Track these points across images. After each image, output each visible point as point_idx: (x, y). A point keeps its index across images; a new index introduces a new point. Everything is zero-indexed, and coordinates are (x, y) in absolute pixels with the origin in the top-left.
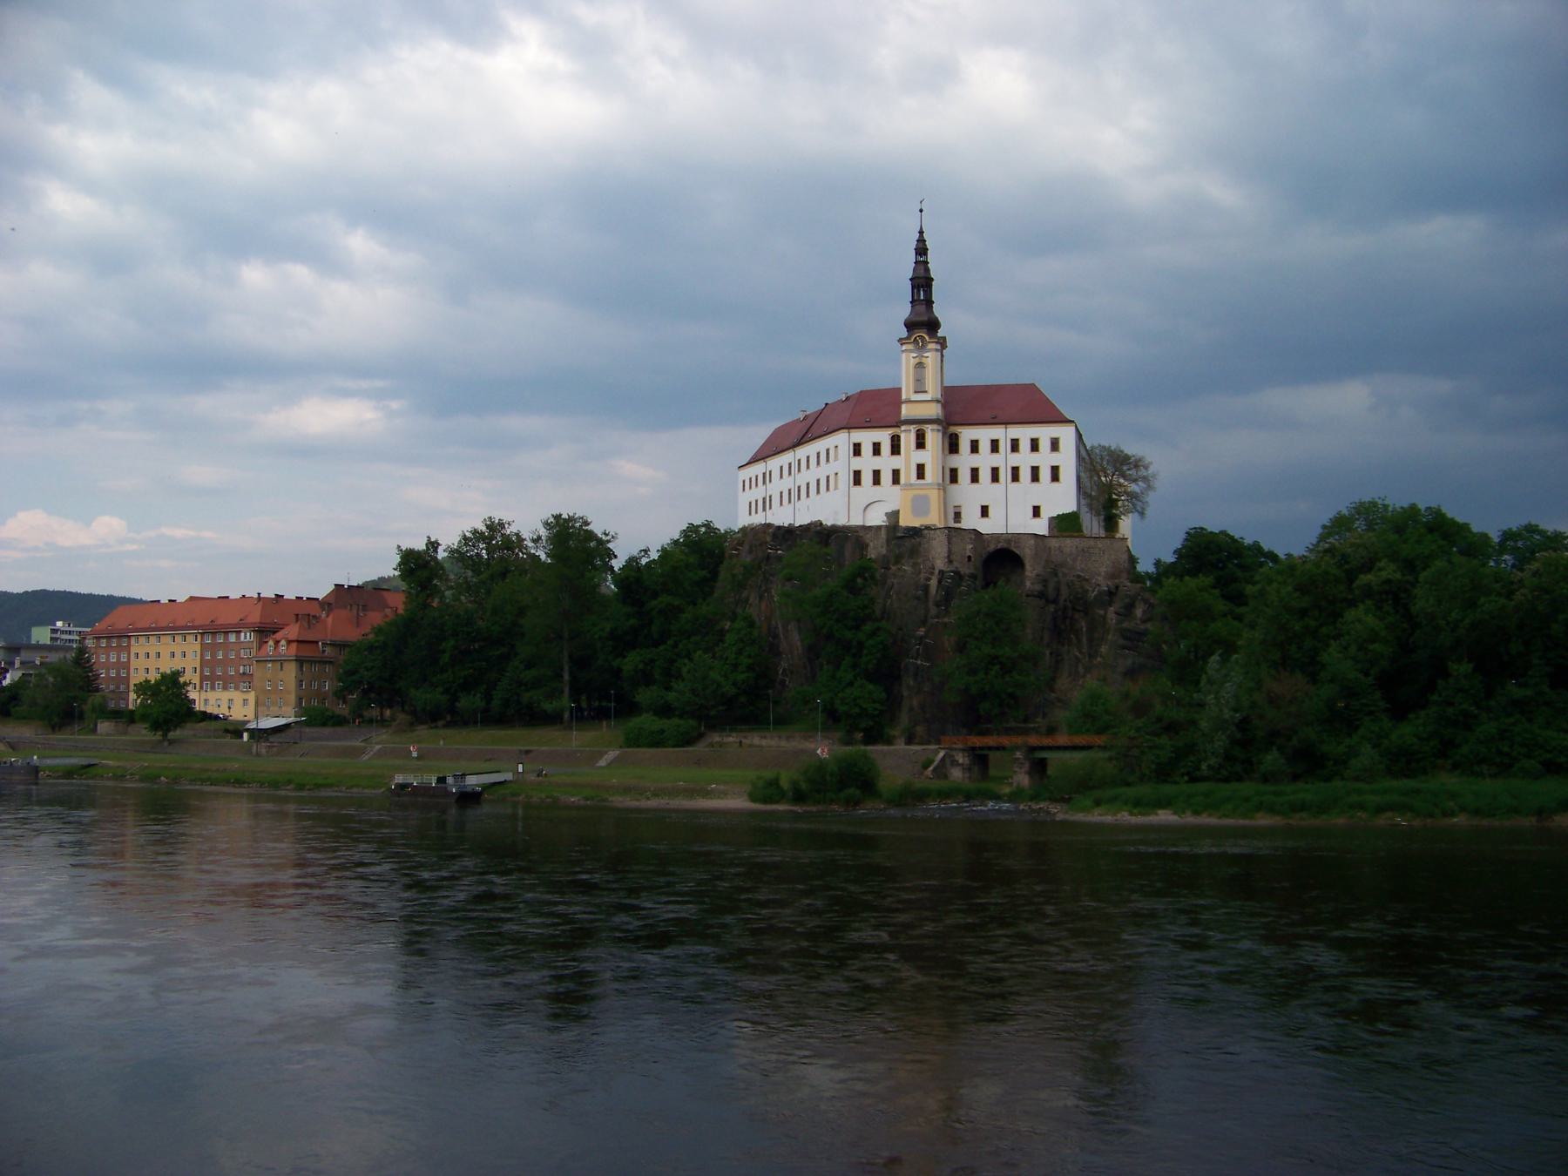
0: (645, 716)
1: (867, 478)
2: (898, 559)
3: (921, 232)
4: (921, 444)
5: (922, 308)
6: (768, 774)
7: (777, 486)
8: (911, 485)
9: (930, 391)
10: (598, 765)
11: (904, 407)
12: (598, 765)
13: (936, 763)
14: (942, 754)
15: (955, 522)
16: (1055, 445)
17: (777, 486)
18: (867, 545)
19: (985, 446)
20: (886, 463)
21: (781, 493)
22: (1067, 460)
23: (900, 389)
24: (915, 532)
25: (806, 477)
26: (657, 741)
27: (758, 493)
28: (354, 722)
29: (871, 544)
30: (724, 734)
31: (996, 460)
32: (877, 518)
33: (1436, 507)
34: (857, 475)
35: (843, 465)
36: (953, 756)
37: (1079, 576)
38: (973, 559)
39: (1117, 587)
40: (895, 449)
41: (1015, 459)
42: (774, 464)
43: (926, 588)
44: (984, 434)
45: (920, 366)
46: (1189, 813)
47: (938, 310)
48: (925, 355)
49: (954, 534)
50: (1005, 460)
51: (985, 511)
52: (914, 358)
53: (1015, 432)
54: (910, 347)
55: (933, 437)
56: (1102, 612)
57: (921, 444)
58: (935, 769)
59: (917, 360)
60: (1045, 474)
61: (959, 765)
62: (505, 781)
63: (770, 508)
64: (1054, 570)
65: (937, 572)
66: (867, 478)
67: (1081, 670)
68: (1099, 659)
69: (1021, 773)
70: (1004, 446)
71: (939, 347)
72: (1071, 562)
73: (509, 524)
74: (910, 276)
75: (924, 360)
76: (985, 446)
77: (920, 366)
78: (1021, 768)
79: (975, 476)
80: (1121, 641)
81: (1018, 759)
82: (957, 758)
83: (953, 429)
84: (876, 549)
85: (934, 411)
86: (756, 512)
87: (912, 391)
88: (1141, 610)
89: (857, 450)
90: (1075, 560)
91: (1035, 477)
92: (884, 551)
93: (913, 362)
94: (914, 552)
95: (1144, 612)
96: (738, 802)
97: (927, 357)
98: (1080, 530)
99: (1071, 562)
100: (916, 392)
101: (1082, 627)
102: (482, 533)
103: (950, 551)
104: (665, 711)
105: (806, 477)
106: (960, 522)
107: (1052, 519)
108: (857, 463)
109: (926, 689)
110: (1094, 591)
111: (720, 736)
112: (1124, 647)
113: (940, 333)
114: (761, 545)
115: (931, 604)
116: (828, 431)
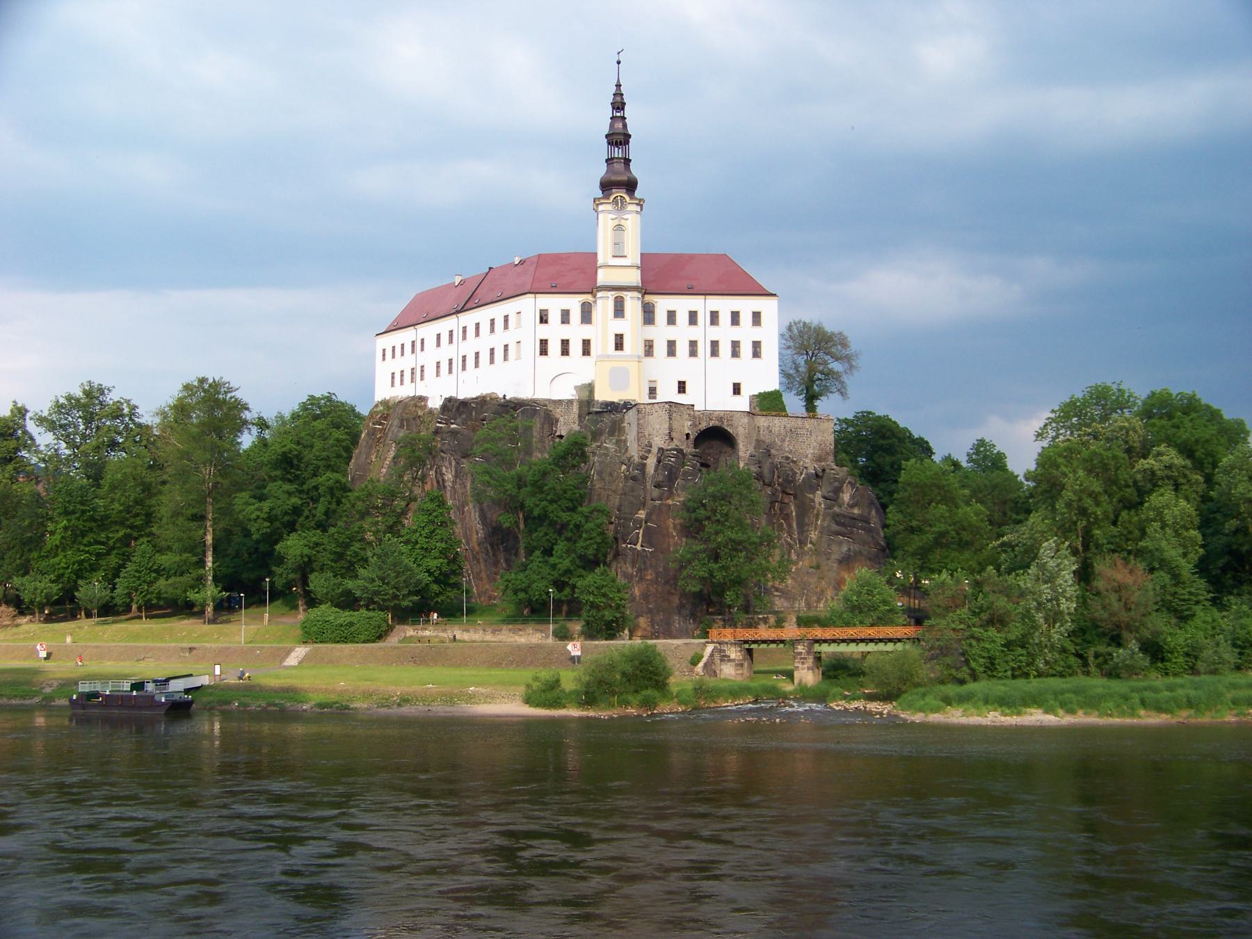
0: (323, 607)
1: (554, 347)
2: (596, 435)
3: (618, 86)
4: (619, 311)
5: (619, 166)
6: (545, 674)
7: (429, 357)
8: (608, 356)
9: (629, 256)
10: (286, 664)
11: (600, 272)
12: (286, 664)
13: (704, 660)
14: (710, 648)
15: (650, 398)
16: (757, 318)
17: (429, 357)
18: (557, 421)
19: (683, 318)
20: (576, 332)
21: (393, 374)
22: (770, 335)
23: (596, 254)
24: (616, 409)
25: (470, 347)
26: (345, 635)
27: (406, 362)
28: (42, 612)
29: (561, 419)
30: (417, 627)
31: (695, 333)
32: (565, 391)
33: (1190, 393)
34: (544, 343)
35: (526, 331)
36: (724, 651)
37: (787, 458)
38: (691, 437)
39: (824, 470)
40: (586, 317)
41: (714, 333)
42: (428, 331)
43: (642, 467)
44: (683, 305)
45: (619, 228)
46: (1061, 712)
47: (636, 170)
48: (625, 217)
49: (675, 409)
50: (703, 333)
51: (682, 387)
52: (612, 219)
53: (715, 303)
54: (609, 207)
55: (633, 304)
56: (811, 496)
57: (619, 311)
58: (706, 665)
59: (616, 222)
60: (746, 349)
61: (730, 660)
62: (202, 686)
63: (422, 379)
64: (765, 451)
65: (655, 450)
66: (554, 347)
67: (794, 557)
68: (809, 545)
69: (803, 669)
70: (704, 318)
71: (638, 209)
72: (779, 443)
73: (109, 390)
74: (606, 133)
75: (623, 222)
76: (683, 318)
77: (619, 228)
78: (803, 663)
79: (671, 348)
80: (835, 527)
81: (800, 653)
82: (728, 653)
83: (648, 298)
84: (568, 425)
85: (634, 278)
86: (402, 383)
87: (610, 256)
88: (848, 494)
89: (544, 319)
90: (783, 441)
91: (715, 351)
92: (576, 427)
93: (611, 224)
94: (617, 429)
95: (852, 497)
96: (512, 707)
98: (784, 409)
99: (779, 443)
100: (614, 256)
101: (792, 512)
102: (78, 400)
103: (671, 429)
104: (348, 602)
105: (470, 347)
106: (655, 398)
107: (753, 398)
108: (544, 331)
109: (649, 577)
110: (801, 474)
111: (414, 630)
112: (838, 533)
113: (637, 194)
114: (414, 419)
115: (649, 485)
116: (480, 303)
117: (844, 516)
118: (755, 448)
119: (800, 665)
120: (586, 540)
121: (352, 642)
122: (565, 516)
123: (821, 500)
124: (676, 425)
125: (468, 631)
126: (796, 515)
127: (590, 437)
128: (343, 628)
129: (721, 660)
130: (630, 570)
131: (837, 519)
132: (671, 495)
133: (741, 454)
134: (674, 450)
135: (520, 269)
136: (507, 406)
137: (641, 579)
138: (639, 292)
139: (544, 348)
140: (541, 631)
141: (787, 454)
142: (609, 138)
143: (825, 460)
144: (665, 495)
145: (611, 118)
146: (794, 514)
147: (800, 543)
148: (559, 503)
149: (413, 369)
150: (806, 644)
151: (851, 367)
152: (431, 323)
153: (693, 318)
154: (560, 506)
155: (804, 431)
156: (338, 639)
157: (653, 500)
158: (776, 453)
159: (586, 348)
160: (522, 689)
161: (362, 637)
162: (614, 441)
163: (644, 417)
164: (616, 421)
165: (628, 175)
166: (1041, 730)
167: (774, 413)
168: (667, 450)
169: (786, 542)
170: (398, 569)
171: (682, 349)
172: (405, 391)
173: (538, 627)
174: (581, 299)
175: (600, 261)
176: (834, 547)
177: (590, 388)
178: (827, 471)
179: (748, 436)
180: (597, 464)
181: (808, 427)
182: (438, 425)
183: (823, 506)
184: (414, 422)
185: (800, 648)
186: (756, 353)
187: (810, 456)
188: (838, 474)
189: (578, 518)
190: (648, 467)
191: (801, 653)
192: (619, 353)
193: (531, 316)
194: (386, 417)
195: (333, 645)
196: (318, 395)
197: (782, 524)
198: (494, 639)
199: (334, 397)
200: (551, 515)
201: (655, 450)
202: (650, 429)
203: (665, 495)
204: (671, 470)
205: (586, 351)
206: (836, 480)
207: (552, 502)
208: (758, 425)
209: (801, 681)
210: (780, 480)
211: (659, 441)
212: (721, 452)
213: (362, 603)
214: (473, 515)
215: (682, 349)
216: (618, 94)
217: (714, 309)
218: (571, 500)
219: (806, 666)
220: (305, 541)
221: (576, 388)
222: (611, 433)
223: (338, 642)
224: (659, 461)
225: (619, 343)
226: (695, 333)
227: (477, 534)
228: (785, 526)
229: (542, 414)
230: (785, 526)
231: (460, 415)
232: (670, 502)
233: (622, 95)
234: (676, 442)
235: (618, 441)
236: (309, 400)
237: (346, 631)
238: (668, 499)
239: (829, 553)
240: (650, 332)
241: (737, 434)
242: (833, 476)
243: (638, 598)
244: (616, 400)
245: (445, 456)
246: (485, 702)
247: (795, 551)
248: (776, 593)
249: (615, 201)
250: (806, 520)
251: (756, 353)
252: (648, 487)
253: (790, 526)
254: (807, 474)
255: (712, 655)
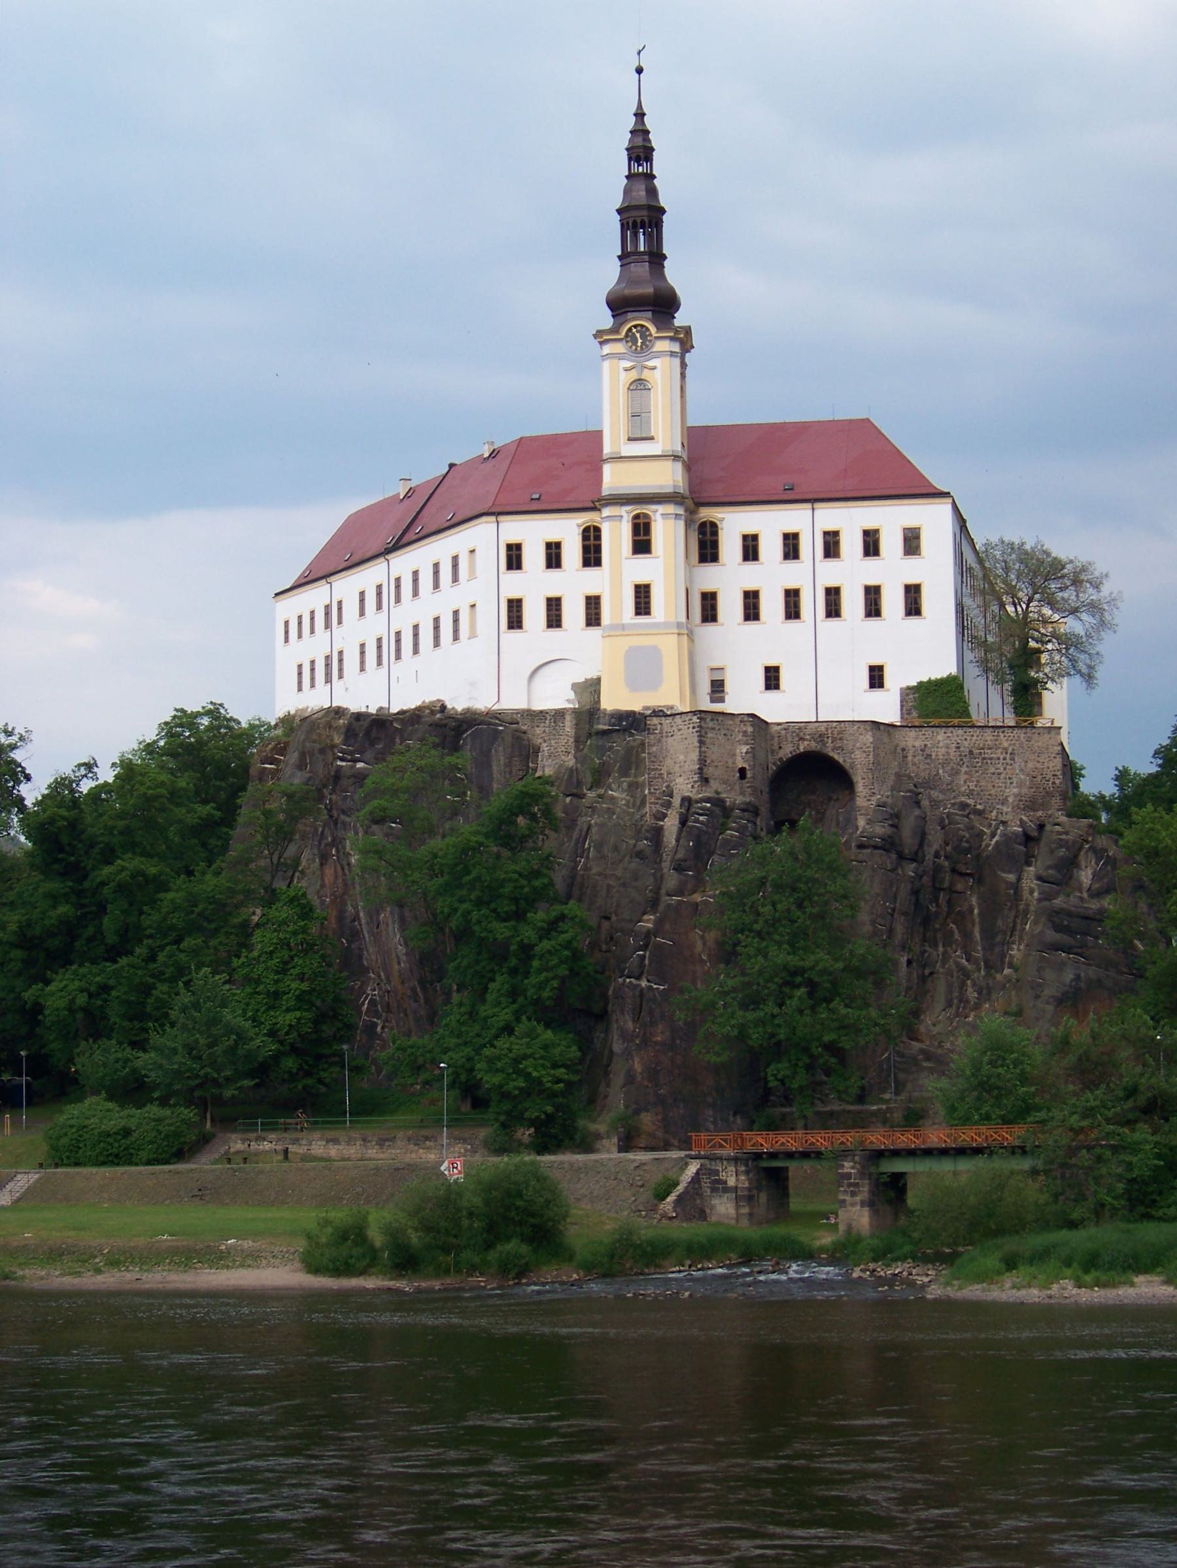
1: (535, 614)
2: (600, 777)
3: (640, 115)
4: (642, 546)
5: (642, 269)
6: (340, 1215)
8: (624, 627)
11: (607, 469)
13: (680, 1188)
14: (693, 1168)
15: (713, 701)
18: (537, 750)
19: (770, 547)
23: (599, 434)
25: (407, 614)
27: (316, 647)
29: (544, 747)
31: (795, 574)
36: (717, 1173)
37: (964, 806)
39: (1041, 827)
40: (592, 556)
41: (831, 573)
42: (347, 586)
45: (639, 385)
47: (675, 274)
48: (650, 364)
49: (711, 724)
51: (772, 678)
52: (626, 370)
53: (831, 516)
54: (620, 348)
57: (642, 546)
58: (680, 1198)
59: (634, 375)
60: (893, 601)
61: (727, 1190)
65: (676, 801)
67: (971, 994)
69: (853, 1205)
70: (812, 545)
71: (676, 347)
74: (618, 207)
75: (646, 374)
76: (770, 547)
77: (639, 385)
78: (853, 1194)
79: (751, 607)
80: (1052, 936)
83: (707, 514)
85: (670, 477)
87: (623, 437)
88: (1090, 872)
89: (514, 557)
90: (955, 773)
92: (570, 761)
93: (625, 378)
94: (632, 762)
97: (654, 368)
98: (965, 713)
100: (629, 439)
101: (971, 911)
103: (703, 762)
105: (407, 614)
106: (722, 700)
107: (907, 692)
108: (514, 584)
110: (993, 835)
111: (243, 1141)
112: (1056, 947)
113: (680, 319)
114: (322, 751)
117: (1070, 914)
118: (892, 790)
119: (848, 1198)
120: (540, 971)
121: (131, 1163)
122: (502, 930)
123: (1034, 884)
124: (714, 753)
125: (335, 1141)
126: (980, 914)
127: (589, 779)
128: (110, 1140)
129: (714, 1190)
130: (630, 1025)
131: (1056, 919)
132: (699, 884)
133: (860, 801)
134: (708, 800)
135: (492, 462)
136: (445, 725)
137: (645, 1042)
138: (677, 503)
139: (515, 615)
140: (465, 1140)
141: (963, 799)
142: (626, 215)
143: (1044, 806)
144: (689, 886)
145: (627, 177)
146: (976, 911)
147: (988, 966)
148: (493, 906)
149: (327, 657)
150: (857, 1158)
151: (1102, 623)
152: (850, 504)
153: (791, 547)
154: (494, 911)
155: (999, 753)
156: (101, 1159)
157: (669, 895)
158: (941, 797)
159: (593, 610)
160: (301, 1245)
161: (144, 1155)
162: (625, 785)
163: (659, 741)
164: (632, 748)
165: (660, 284)
166: (1049, 1314)
167: (935, 722)
168: (697, 802)
169: (958, 964)
170: (214, 1031)
171: (772, 605)
172: (316, 699)
173: (330, 1134)
174: (580, 521)
175: (607, 449)
176: (1049, 974)
177: (593, 687)
178: (1048, 828)
179: (877, 766)
180: (594, 830)
181: (1006, 744)
182: (339, 763)
183: (1036, 894)
184: (321, 757)
185: (848, 1167)
186: (913, 606)
187: (1010, 800)
188: (1067, 833)
189: (528, 933)
190: (666, 833)
191: (848, 1176)
192: (643, 619)
193: (491, 557)
194: (285, 748)
195: (94, 1170)
196: (193, 707)
197: (952, 932)
198: (381, 1156)
199: (222, 711)
200: (477, 928)
201: (676, 801)
202: (669, 762)
203: (689, 886)
204: (699, 836)
205: (593, 616)
206: (1062, 844)
207: (479, 903)
208: (903, 744)
209: (850, 1227)
210: (949, 848)
211: (684, 786)
212: (830, 799)
213: (156, 1095)
214: (390, 928)
215: (772, 605)
216: (640, 132)
217: (831, 527)
218: (516, 900)
219: (858, 1199)
220: (83, 984)
221: (575, 686)
222: (624, 772)
223: (103, 1164)
224: (683, 822)
225: (642, 598)
226: (795, 574)
227: (399, 963)
228: (957, 936)
229: (509, 739)
230: (957, 936)
231: (372, 744)
232: (698, 898)
233: (648, 132)
234: (715, 785)
235: (630, 785)
236: (174, 717)
237: (116, 1145)
238: (694, 892)
239: (1040, 985)
240: (710, 577)
241: (852, 766)
242: (1055, 837)
243: (639, 1078)
244: (637, 708)
245: (348, 819)
246: (242, 1266)
247: (974, 984)
248: (925, 1064)
249: (630, 337)
250: (999, 923)
251: (913, 606)
252: (665, 870)
253: (967, 936)
254: (1003, 835)
255: (696, 1179)
